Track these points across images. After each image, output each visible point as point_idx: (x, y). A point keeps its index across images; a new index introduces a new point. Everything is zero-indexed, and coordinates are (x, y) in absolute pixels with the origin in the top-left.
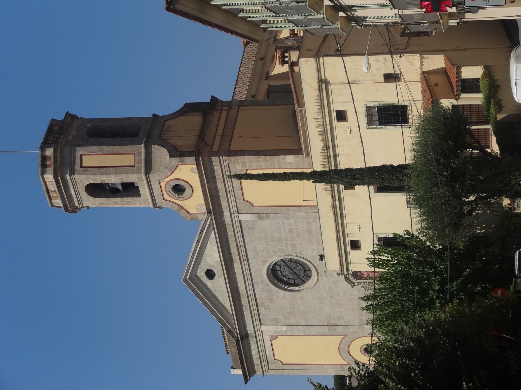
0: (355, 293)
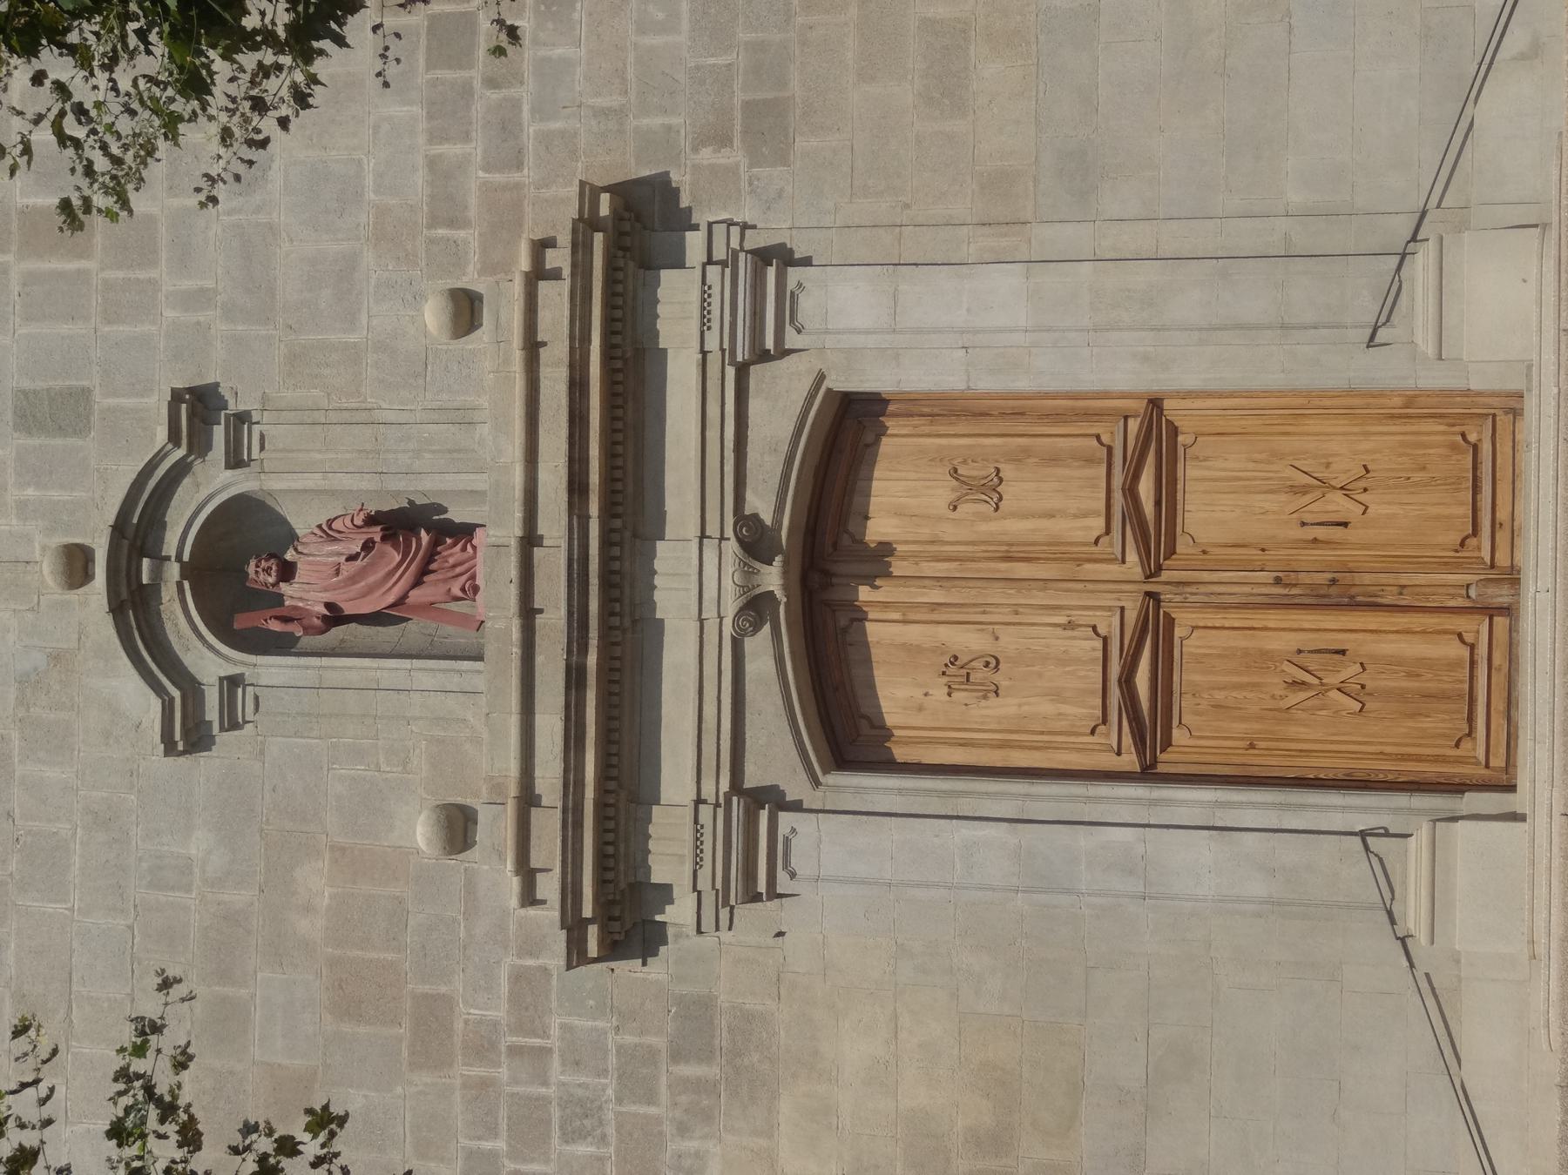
0: (199, 844)
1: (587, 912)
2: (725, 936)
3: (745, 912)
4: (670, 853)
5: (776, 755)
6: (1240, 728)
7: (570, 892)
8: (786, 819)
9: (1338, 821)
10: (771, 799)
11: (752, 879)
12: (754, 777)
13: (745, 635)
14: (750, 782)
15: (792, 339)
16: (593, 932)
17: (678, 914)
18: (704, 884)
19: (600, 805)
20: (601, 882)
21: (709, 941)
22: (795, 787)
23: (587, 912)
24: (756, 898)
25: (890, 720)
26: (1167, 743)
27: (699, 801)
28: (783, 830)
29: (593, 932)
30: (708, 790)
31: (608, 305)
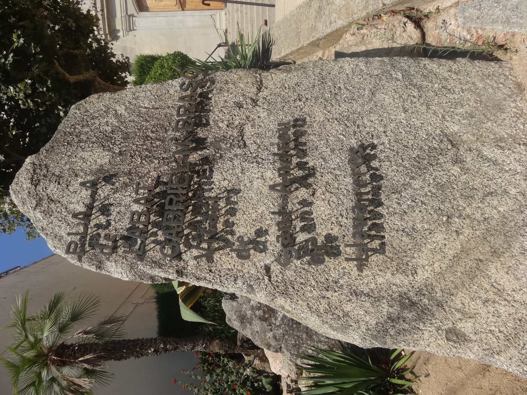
1: (107, 33)
2: (127, 37)
3: (130, 33)
4: (118, 25)
5: (132, 9)
6: (195, 4)
7: (105, 30)
8: (134, 18)
9: (207, 14)
10: (133, 16)
11: (130, 28)
12: (129, 13)
13: (156, 340)
14: (129, 13)
15: (135, 28)
16: (108, 36)
17: (120, 34)
18: (124, 29)
19: (108, 17)
20: (109, 29)
21: (125, 38)
22: (135, 14)
23: (107, 33)
24: (131, 30)
25: (149, 6)
26: (185, 7)
27: (122, 16)
28: (134, 20)
29: (108, 36)
30: (123, 15)
31: (108, 21)
